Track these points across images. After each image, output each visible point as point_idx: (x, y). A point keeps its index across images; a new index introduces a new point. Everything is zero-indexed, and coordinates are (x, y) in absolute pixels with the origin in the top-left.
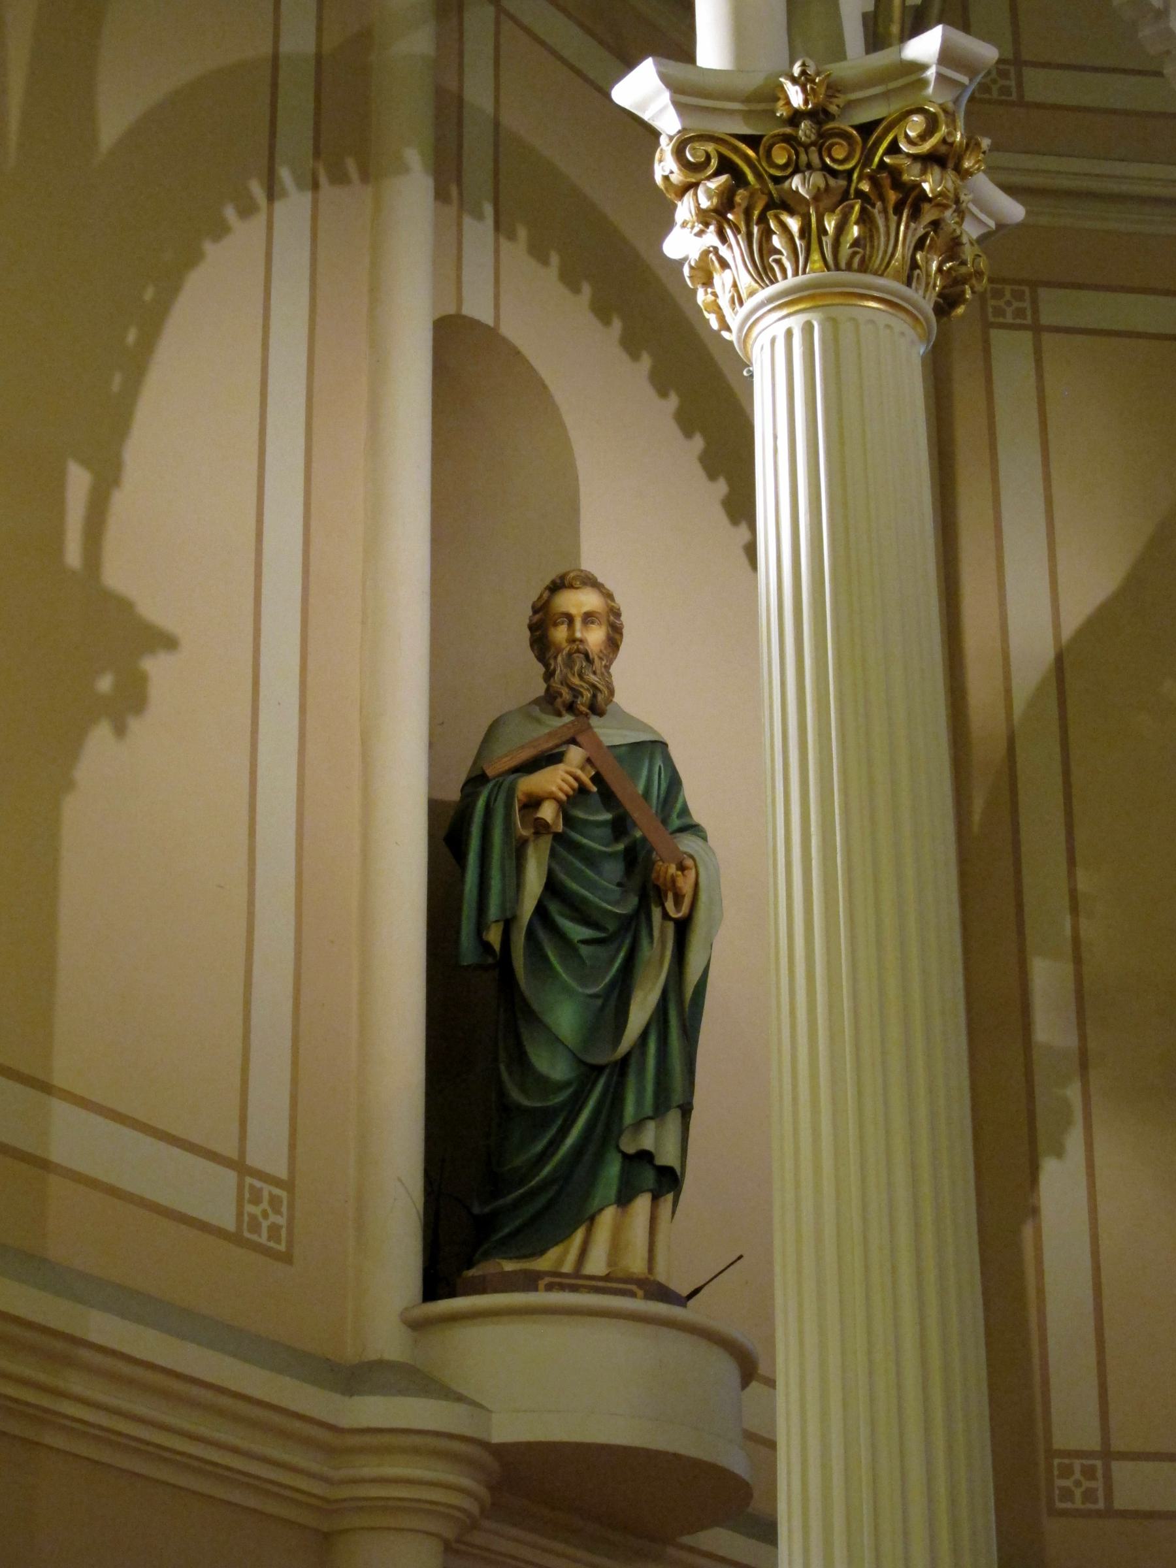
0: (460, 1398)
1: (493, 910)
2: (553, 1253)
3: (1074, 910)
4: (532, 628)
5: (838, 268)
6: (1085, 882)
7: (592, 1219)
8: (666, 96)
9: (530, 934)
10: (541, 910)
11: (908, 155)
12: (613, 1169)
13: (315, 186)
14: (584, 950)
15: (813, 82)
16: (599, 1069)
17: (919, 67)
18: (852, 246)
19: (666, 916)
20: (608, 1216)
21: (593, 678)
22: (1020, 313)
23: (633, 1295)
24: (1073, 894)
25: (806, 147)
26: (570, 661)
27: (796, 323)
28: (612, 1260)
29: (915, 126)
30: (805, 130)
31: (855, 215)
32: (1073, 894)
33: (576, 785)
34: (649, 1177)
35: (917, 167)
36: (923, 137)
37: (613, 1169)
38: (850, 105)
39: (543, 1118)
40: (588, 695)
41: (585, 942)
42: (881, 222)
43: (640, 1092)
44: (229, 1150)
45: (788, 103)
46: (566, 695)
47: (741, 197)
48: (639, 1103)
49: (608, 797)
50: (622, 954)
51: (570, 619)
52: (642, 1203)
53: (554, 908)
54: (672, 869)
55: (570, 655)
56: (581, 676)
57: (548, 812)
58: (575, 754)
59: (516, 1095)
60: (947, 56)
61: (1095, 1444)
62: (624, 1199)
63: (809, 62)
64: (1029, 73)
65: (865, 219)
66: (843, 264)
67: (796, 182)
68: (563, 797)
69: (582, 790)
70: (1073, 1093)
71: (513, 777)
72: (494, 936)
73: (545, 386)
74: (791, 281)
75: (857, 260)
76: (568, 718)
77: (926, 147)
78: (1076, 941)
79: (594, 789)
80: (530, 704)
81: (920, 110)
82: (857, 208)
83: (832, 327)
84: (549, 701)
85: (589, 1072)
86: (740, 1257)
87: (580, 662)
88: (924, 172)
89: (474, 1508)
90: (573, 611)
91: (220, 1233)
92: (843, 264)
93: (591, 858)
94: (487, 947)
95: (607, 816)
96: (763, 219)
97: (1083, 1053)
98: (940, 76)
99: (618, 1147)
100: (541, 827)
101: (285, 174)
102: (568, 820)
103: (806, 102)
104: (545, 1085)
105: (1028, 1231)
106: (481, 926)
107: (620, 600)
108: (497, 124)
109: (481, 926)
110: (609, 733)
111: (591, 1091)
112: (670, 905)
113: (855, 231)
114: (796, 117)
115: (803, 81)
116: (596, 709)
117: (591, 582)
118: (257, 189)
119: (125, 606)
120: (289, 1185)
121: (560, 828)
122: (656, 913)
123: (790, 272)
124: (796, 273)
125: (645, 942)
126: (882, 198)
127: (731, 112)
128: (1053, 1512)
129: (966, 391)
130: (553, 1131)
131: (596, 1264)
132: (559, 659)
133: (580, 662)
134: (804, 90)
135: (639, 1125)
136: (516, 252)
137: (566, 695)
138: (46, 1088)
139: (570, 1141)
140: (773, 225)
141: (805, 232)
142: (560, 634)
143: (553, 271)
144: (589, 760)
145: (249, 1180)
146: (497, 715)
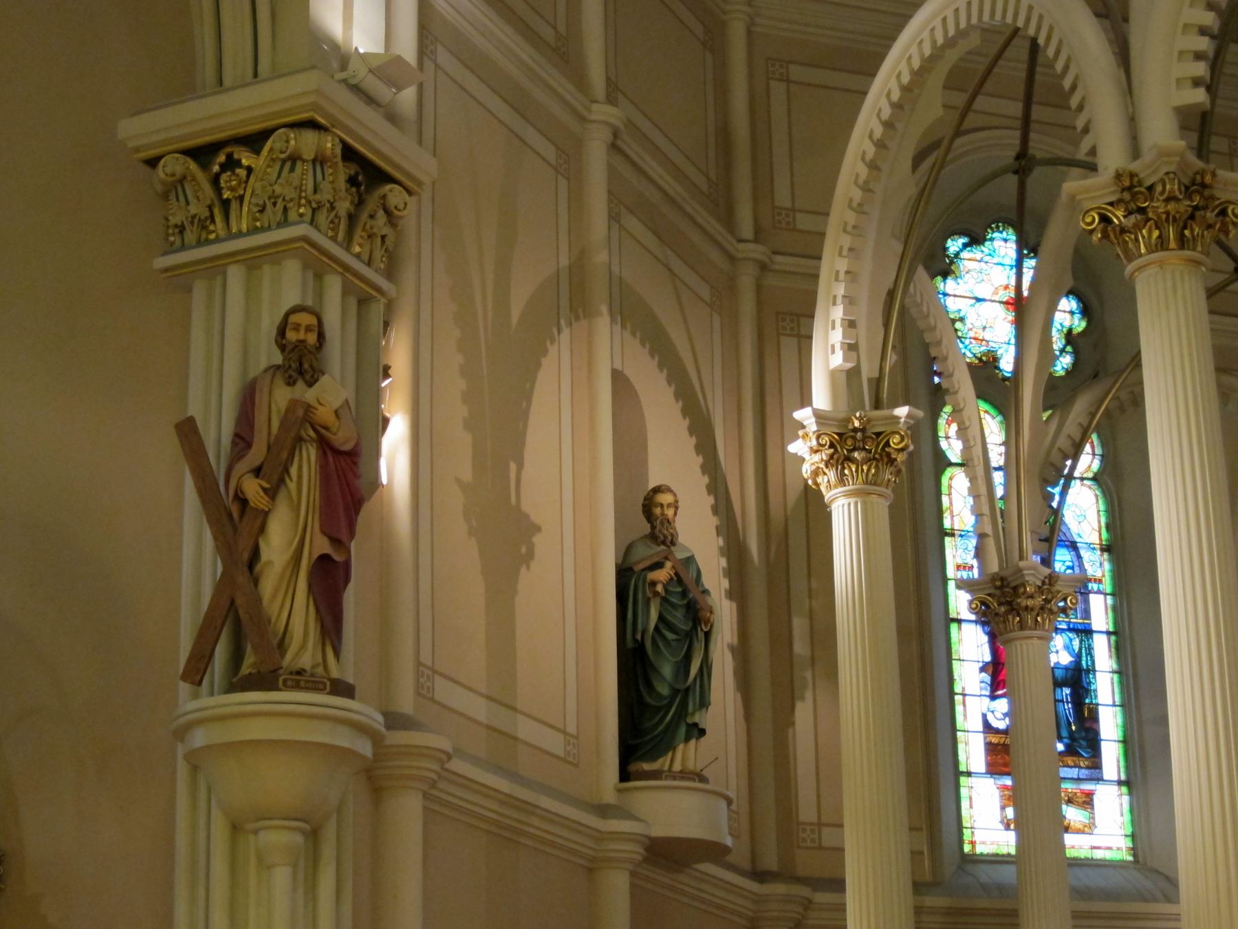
0: (641, 821)
1: (640, 627)
2: (661, 761)
3: (810, 597)
4: (644, 506)
5: (867, 484)
6: (814, 585)
7: (674, 749)
8: (813, 420)
9: (653, 638)
10: (656, 628)
11: (893, 448)
12: (683, 730)
13: (571, 324)
14: (674, 644)
15: (863, 419)
16: (678, 691)
17: (898, 418)
18: (872, 476)
19: (702, 630)
20: (681, 746)
21: (672, 531)
22: (792, 329)
23: (694, 781)
24: (810, 590)
25: (859, 441)
26: (662, 523)
27: (852, 500)
28: (683, 765)
29: (896, 439)
30: (859, 435)
31: (873, 466)
32: (810, 590)
33: (668, 576)
34: (696, 732)
35: (896, 453)
36: (899, 443)
37: (683, 730)
38: (874, 426)
39: (659, 709)
40: (670, 538)
41: (673, 640)
42: (881, 468)
43: (694, 699)
44: (561, 726)
45: (853, 424)
46: (662, 538)
47: (835, 457)
48: (694, 704)
49: (680, 581)
50: (686, 647)
51: (662, 506)
52: (693, 742)
53: (661, 626)
54: (708, 614)
55: (662, 520)
56: (667, 529)
57: (659, 588)
58: (668, 564)
59: (649, 700)
60: (909, 416)
61: (815, 820)
62: (687, 740)
63: (862, 413)
64: (799, 216)
65: (877, 467)
66: (869, 482)
67: (856, 454)
68: (665, 582)
69: (671, 579)
70: (808, 675)
71: (644, 573)
72: (639, 637)
73: (628, 380)
74: (851, 487)
75: (873, 482)
76: (663, 547)
77: (900, 446)
78: (811, 611)
79: (675, 578)
80: (642, 538)
81: (898, 433)
82: (874, 464)
83: (864, 504)
84: (653, 537)
85: (675, 692)
86: (717, 759)
87: (666, 524)
88: (898, 454)
89: (442, 785)
90: (664, 503)
91: (557, 757)
92: (869, 482)
93: (673, 606)
94: (635, 640)
95: (679, 589)
96: (842, 464)
97: (813, 659)
98: (905, 422)
99: (685, 721)
100: (656, 594)
101: (562, 322)
102: (666, 591)
103: (860, 426)
104: (660, 696)
105: (790, 731)
106: (634, 634)
107: (679, 497)
108: (620, 278)
109: (634, 634)
110: (680, 555)
111: (675, 700)
112: (703, 626)
113: (873, 471)
114: (855, 430)
115: (860, 419)
116: (673, 543)
117: (669, 490)
118: (555, 331)
119: (527, 517)
120: (576, 738)
121: (663, 594)
122: (699, 629)
123: (851, 483)
124: (853, 484)
125: (695, 641)
126: (882, 459)
127: (831, 425)
128: (799, 847)
129: (770, 363)
130: (660, 715)
131: (677, 767)
132: (658, 521)
133: (666, 524)
134: (860, 421)
135: (693, 714)
136: (627, 334)
137: (662, 538)
138: (514, 709)
139: (668, 718)
140: (845, 465)
141: (857, 471)
142: (658, 511)
143: (647, 350)
144: (673, 567)
145: (567, 737)
146: (630, 541)
